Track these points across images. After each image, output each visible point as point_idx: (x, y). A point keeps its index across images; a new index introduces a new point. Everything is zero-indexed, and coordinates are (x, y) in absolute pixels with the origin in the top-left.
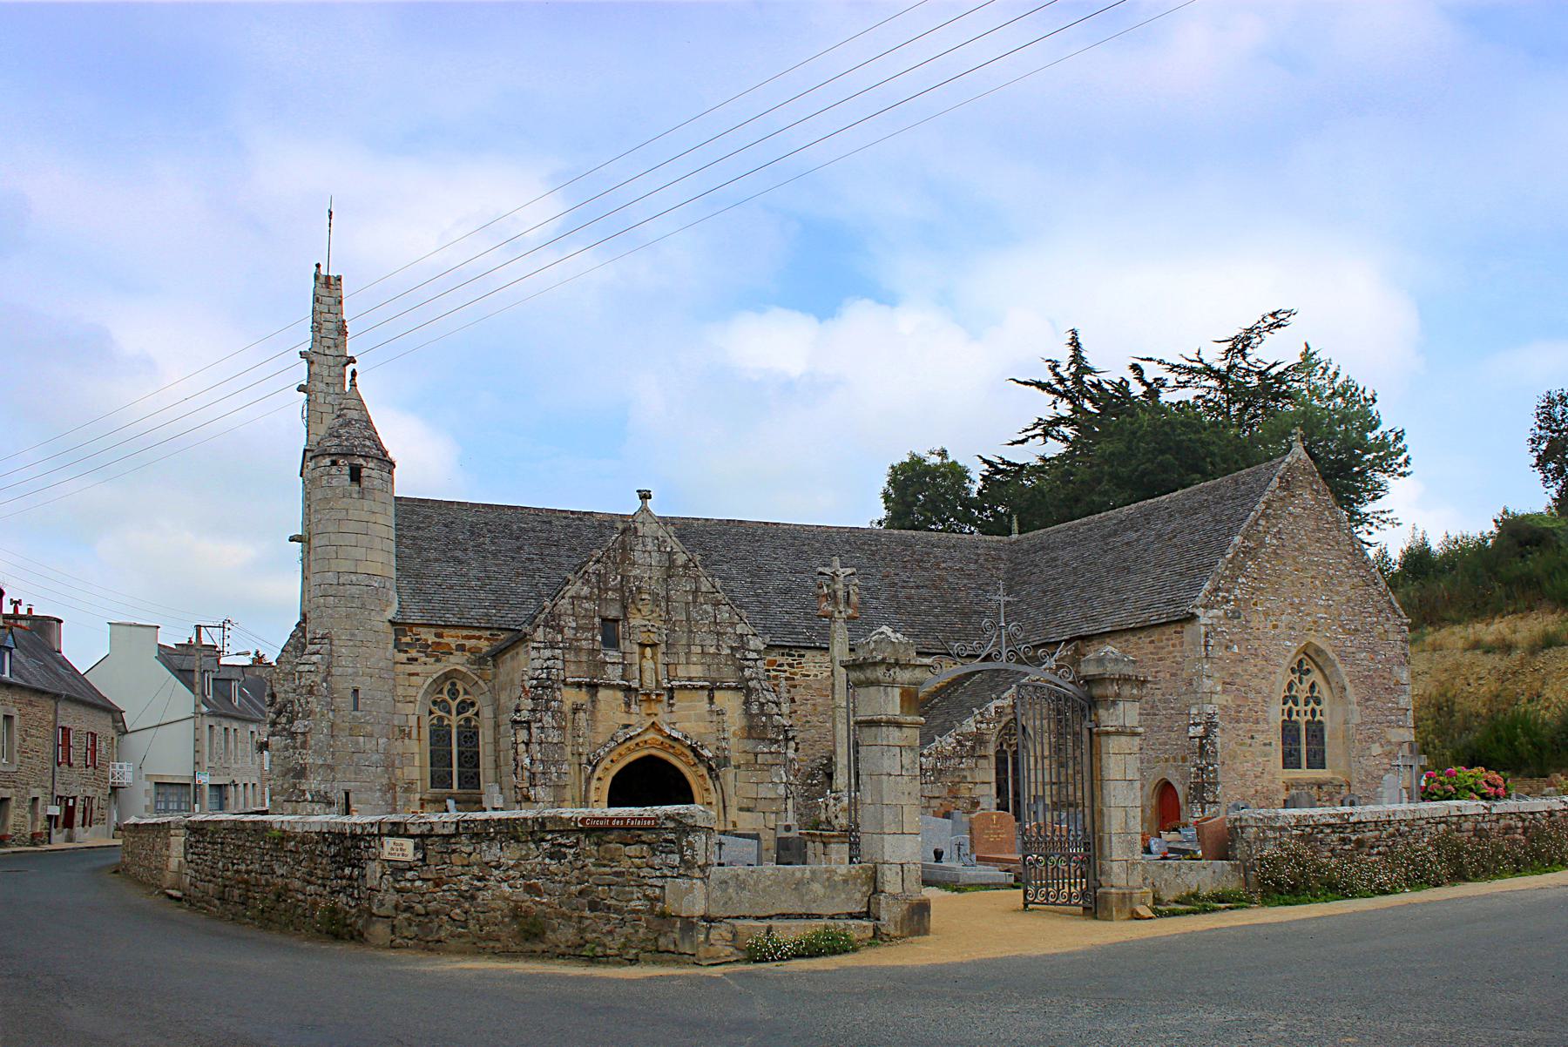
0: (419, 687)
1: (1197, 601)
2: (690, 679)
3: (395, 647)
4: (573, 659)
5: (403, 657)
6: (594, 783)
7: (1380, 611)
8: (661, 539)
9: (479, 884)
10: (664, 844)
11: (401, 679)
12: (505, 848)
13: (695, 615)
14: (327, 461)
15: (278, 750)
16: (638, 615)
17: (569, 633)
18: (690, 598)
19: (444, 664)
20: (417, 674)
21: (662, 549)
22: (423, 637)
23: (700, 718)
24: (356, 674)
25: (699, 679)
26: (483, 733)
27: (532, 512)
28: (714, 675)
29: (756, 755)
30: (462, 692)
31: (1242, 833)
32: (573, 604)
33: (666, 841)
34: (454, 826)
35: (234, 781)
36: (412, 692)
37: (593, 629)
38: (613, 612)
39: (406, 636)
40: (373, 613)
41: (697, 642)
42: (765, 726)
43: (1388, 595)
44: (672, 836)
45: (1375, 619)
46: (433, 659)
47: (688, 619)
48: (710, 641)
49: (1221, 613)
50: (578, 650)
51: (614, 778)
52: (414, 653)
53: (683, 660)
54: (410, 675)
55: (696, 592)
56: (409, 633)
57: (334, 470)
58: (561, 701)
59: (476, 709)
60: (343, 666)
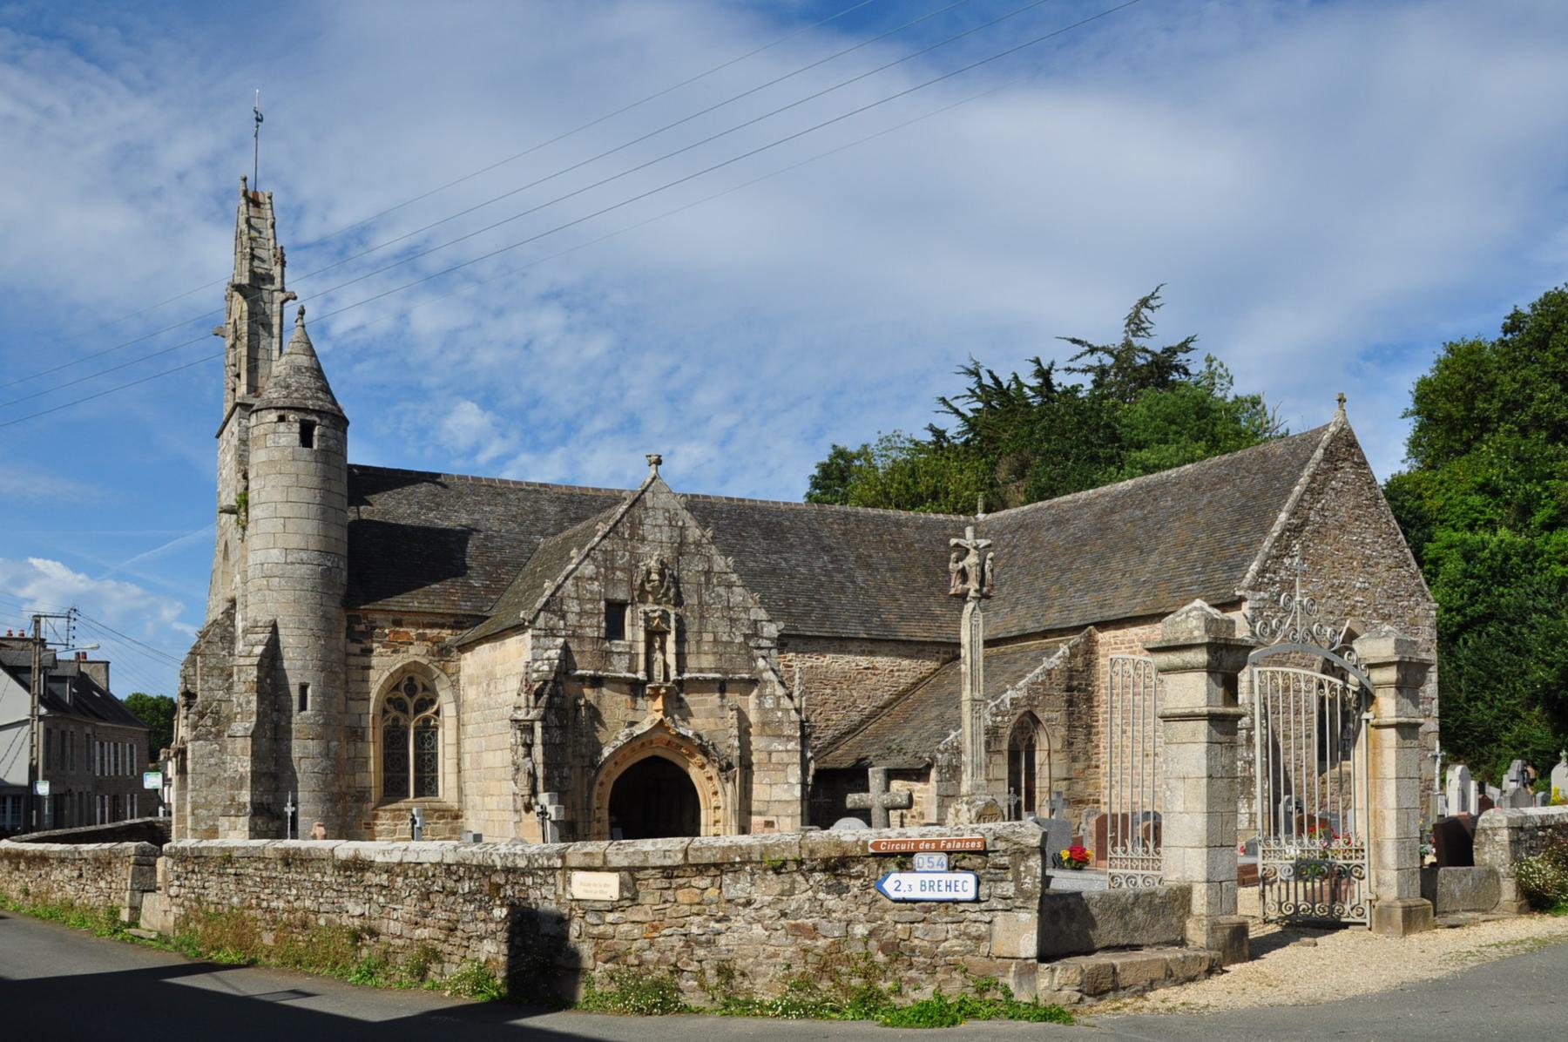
1: (1245, 583)
2: (701, 670)
3: (347, 637)
6: (597, 788)
7: (1411, 596)
8: (672, 513)
9: (717, 926)
10: (992, 871)
12: (759, 882)
13: (708, 598)
14: (273, 416)
15: (202, 756)
17: (572, 619)
18: (703, 579)
19: (401, 655)
21: (674, 523)
25: (711, 670)
26: (443, 733)
27: (484, 483)
28: (727, 666)
29: (770, 754)
30: (420, 688)
31: (1495, 835)
32: (577, 586)
33: (996, 867)
34: (680, 856)
35: (70, 790)
37: (599, 614)
39: (360, 623)
41: (709, 629)
43: (1418, 577)
44: (1005, 860)
45: (1406, 603)
46: (390, 650)
47: (700, 603)
49: (1266, 596)
51: (615, 783)
55: (708, 573)
58: (564, 697)
59: (435, 707)
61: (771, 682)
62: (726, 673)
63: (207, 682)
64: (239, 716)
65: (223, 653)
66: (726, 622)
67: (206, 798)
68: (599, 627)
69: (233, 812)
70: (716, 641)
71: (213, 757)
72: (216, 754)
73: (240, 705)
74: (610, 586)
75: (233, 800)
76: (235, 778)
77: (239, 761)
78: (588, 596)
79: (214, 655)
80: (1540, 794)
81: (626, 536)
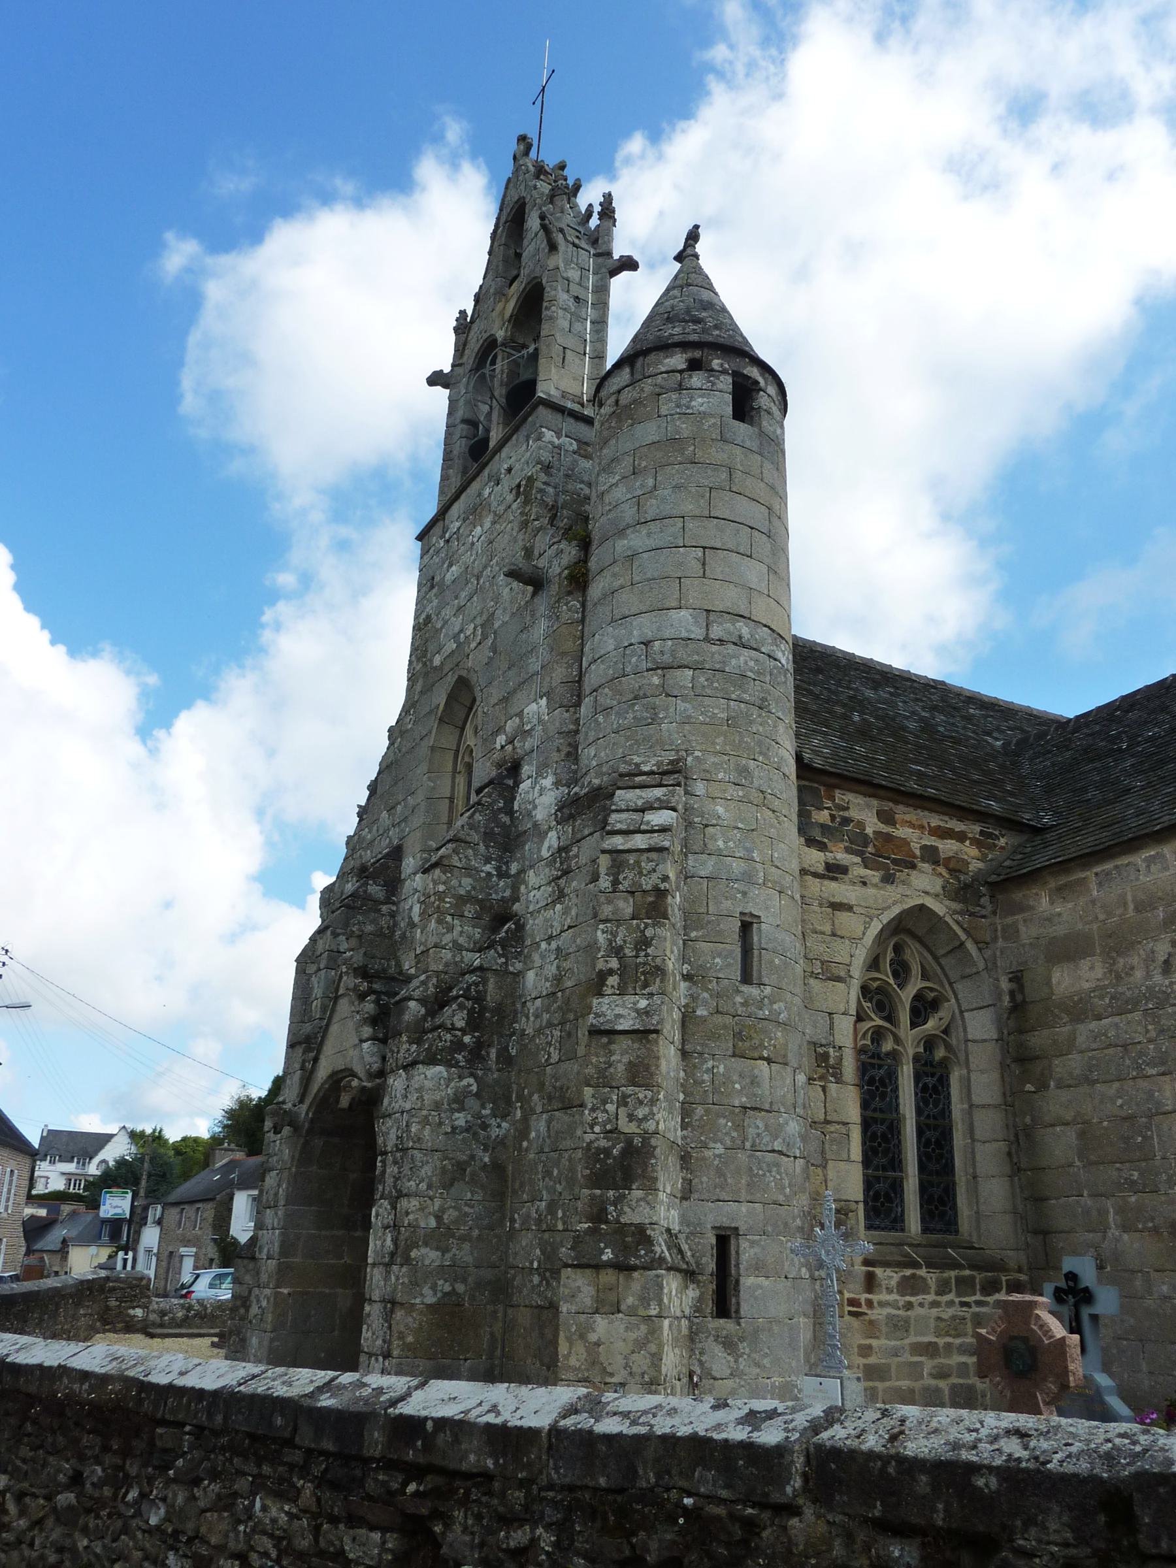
5: (816, 859)
19: (901, 889)
20: (849, 908)
22: (854, 814)
24: (748, 878)
39: (820, 808)
54: (837, 906)
56: (829, 804)
60: (720, 854)
63: (450, 929)
64: (613, 981)
65: (488, 868)
67: (439, 1218)
69: (608, 1255)
73: (617, 951)
75: (598, 1215)
76: (607, 1152)
77: (623, 1101)
79: (468, 870)
80: (1023, 1277)
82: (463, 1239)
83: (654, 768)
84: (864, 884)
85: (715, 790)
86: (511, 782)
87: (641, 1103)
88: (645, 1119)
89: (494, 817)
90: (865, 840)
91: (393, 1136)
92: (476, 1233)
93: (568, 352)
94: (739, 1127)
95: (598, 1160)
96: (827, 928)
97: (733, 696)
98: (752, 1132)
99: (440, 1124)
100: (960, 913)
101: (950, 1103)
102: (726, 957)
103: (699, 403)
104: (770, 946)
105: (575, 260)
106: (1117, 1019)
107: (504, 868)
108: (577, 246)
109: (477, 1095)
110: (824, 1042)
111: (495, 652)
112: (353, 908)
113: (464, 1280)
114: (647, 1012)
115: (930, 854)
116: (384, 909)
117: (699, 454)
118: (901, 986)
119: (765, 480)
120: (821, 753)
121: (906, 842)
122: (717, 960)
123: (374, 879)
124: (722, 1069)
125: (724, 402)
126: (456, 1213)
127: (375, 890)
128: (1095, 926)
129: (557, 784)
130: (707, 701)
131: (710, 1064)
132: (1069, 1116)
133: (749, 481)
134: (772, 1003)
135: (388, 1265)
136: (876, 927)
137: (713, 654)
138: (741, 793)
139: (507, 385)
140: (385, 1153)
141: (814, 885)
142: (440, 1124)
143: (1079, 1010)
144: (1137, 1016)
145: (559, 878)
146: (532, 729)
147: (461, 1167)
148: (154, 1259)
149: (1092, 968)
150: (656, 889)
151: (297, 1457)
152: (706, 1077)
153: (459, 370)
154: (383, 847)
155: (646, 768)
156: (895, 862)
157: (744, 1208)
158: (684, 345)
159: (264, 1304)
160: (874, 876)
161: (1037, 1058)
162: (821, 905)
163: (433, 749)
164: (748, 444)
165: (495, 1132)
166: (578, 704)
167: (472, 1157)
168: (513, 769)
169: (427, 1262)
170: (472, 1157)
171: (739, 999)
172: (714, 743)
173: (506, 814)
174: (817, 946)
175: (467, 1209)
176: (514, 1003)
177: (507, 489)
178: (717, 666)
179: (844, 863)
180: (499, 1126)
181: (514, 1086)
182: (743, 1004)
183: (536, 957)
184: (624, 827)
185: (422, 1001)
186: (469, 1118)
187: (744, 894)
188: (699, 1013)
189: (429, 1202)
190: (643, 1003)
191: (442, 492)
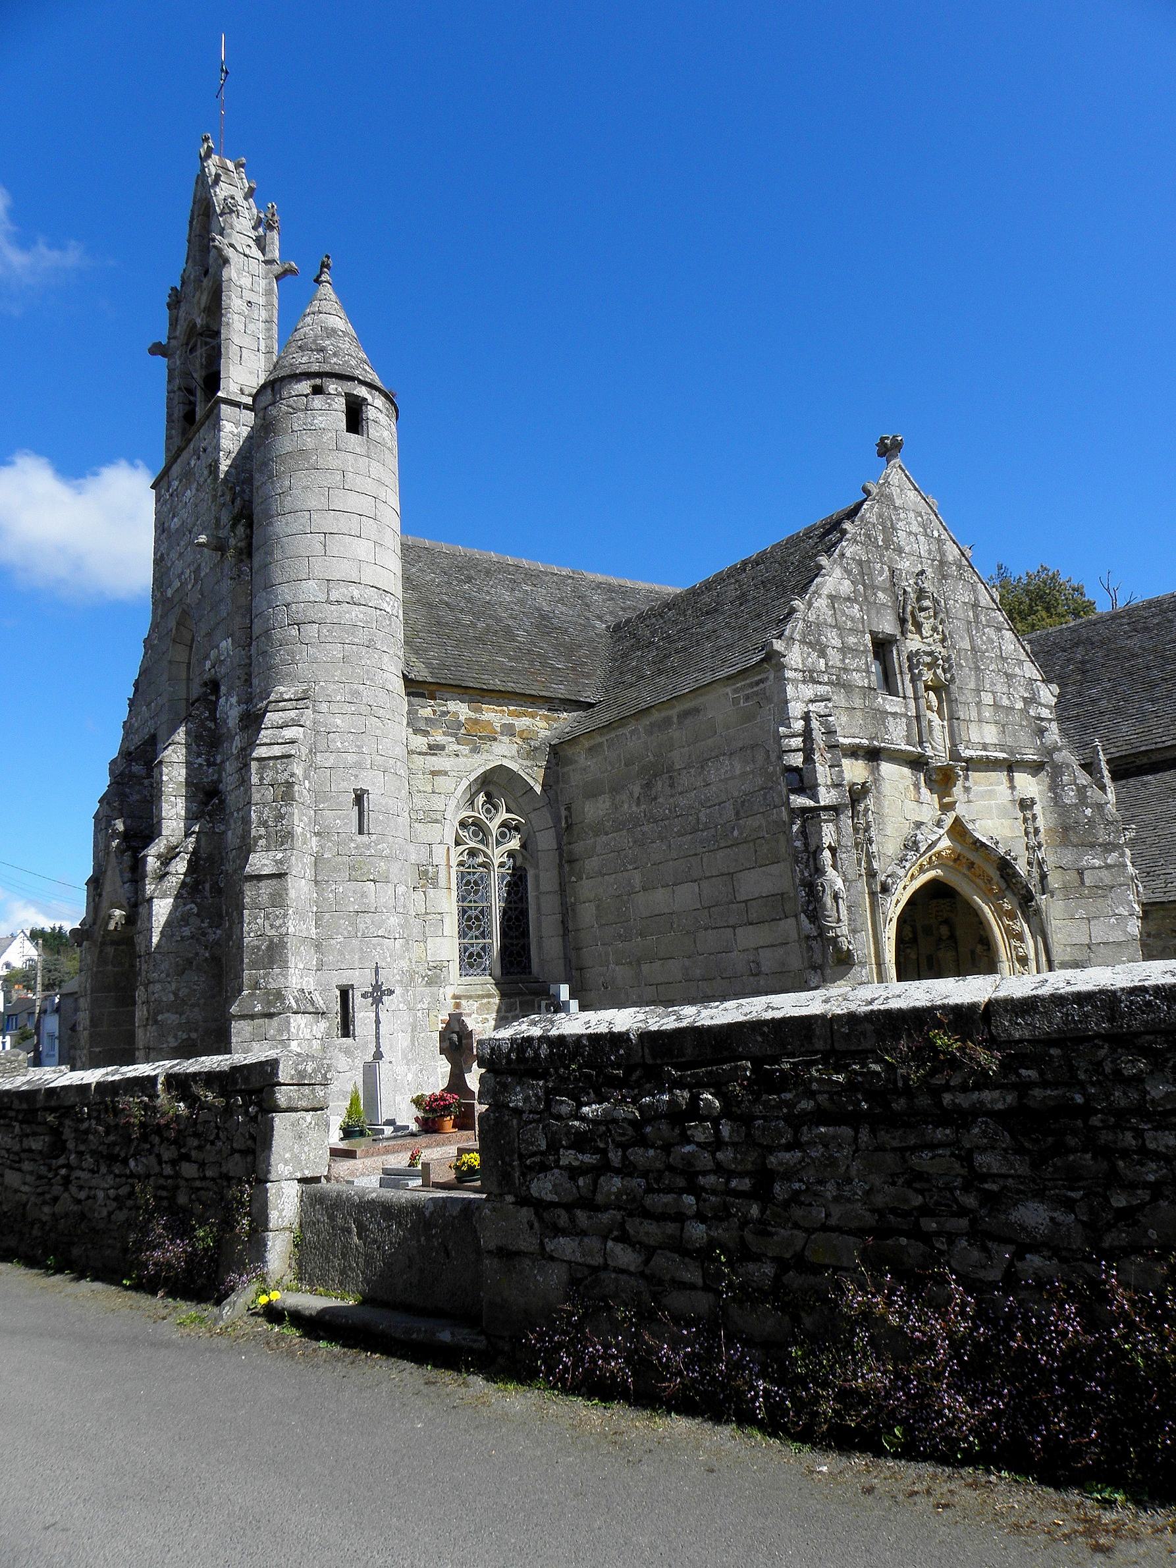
0: (448, 795)
2: (985, 747)
4: (843, 704)
5: (420, 742)
11: (422, 782)
16: (917, 637)
17: (834, 657)
18: (971, 614)
19: (485, 756)
20: (446, 773)
23: (1003, 813)
24: (359, 765)
26: (537, 877)
28: (1009, 741)
29: (1081, 873)
36: (438, 803)
38: (888, 626)
40: (386, 658)
42: (1091, 821)
47: (973, 648)
48: (1001, 688)
50: (847, 687)
51: (904, 920)
52: (439, 738)
53: (974, 715)
54: (434, 773)
57: (318, 401)
61: (1068, 766)
62: (1012, 753)
64: (262, 842)
65: (199, 760)
66: (1003, 679)
67: (176, 994)
68: (868, 672)
70: (996, 706)
71: (187, 924)
72: (192, 920)
73: (264, 824)
74: (873, 612)
76: (258, 948)
77: (267, 917)
78: (849, 624)
81: (880, 543)
82: (193, 1006)
83: (292, 696)
84: (457, 755)
85: (335, 708)
86: (213, 698)
87: (278, 917)
88: (281, 926)
89: (202, 724)
90: (460, 725)
91: (143, 946)
92: (202, 1001)
93: (243, 349)
94: (354, 924)
95: (254, 953)
96: (429, 789)
97: (347, 641)
98: (362, 926)
99: (173, 935)
100: (531, 767)
101: (527, 892)
102: (343, 819)
103: (320, 421)
104: (375, 809)
105: (246, 268)
106: (615, 834)
107: (212, 759)
108: (247, 256)
109: (198, 915)
110: (425, 863)
111: (202, 595)
112: (123, 784)
113: (196, 1031)
114: (281, 862)
115: (509, 730)
116: (146, 782)
117: (321, 461)
118: (491, 819)
119: (372, 476)
120: (421, 672)
121: (489, 723)
122: (338, 821)
123: (136, 761)
124: (341, 890)
125: (340, 420)
126: (187, 990)
127: (137, 768)
128: (606, 775)
129: (239, 703)
130: (328, 646)
131: (333, 887)
132: (592, 897)
133: (359, 479)
134: (376, 845)
135: (145, 1026)
136: (465, 783)
137: (332, 612)
138: (353, 709)
139: (206, 367)
140: (140, 957)
141: (419, 760)
142: (173, 935)
143: (598, 829)
144: (624, 832)
145: (241, 769)
146: (224, 660)
147: (190, 962)
148: (57, 1041)
149: (604, 802)
150: (287, 782)
151: (12, 1114)
152: (330, 895)
153: (174, 342)
154: (145, 734)
155: (286, 697)
156: (480, 738)
157: (357, 972)
158: (308, 375)
159: (84, 1059)
160: (464, 749)
161: (577, 860)
162: (423, 774)
163: (170, 662)
164: (358, 450)
165: (212, 937)
166: (250, 645)
167: (197, 954)
168: (214, 686)
169: (169, 1022)
170: (197, 954)
171: (353, 845)
172: (333, 676)
173: (211, 721)
174: (419, 801)
175: (195, 987)
176: (220, 853)
177: (204, 465)
178: (335, 621)
179: (443, 742)
180: (215, 933)
181: (224, 907)
182: (356, 848)
183: (232, 821)
184: (268, 741)
185: (159, 857)
186: (193, 929)
187: (356, 776)
188: (325, 856)
189: (168, 985)
190: (280, 856)
191: (168, 449)
